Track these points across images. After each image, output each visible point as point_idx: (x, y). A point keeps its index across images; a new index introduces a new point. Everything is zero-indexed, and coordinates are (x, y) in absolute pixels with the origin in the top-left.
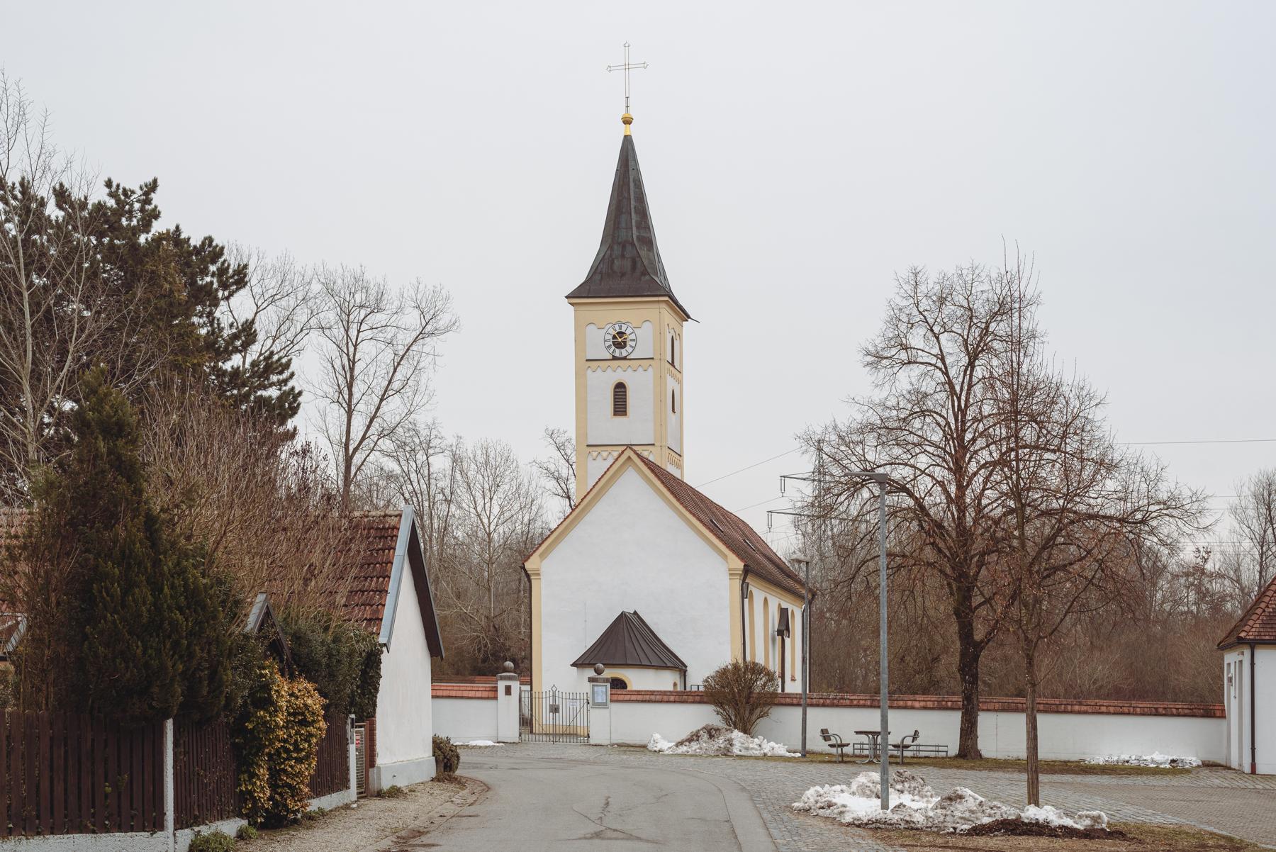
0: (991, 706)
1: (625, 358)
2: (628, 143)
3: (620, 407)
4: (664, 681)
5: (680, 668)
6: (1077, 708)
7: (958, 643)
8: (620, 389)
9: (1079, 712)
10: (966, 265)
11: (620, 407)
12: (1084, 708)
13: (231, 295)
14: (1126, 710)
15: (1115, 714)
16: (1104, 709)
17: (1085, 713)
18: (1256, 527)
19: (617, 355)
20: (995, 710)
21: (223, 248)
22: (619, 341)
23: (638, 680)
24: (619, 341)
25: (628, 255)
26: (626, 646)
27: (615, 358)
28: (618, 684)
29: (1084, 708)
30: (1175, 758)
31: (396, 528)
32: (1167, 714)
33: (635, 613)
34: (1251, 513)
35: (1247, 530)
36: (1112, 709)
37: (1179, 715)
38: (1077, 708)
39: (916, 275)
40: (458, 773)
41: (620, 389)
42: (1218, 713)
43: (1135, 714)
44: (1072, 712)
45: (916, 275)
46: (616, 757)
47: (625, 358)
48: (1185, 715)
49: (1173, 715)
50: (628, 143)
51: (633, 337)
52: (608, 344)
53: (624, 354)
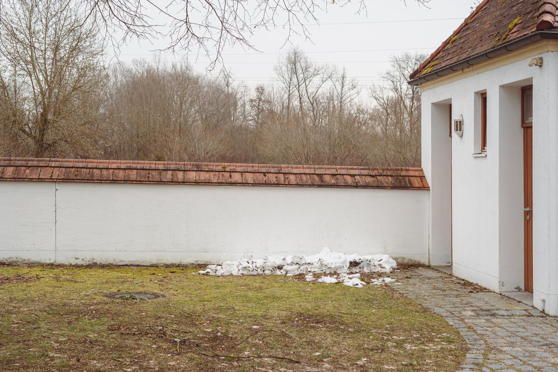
0: (45, 174)
6: (192, 176)
9: (197, 183)
10: (389, 67)
12: (204, 176)
14: (272, 178)
15: (255, 184)
16: (237, 177)
17: (208, 183)
18: (286, 76)
20: (52, 180)
21: (502, 87)
29: (204, 176)
30: (355, 257)
32: (338, 184)
34: (284, 68)
35: (282, 79)
36: (250, 178)
37: (356, 186)
38: (192, 176)
39: (295, 53)
40: (392, 94)
42: (416, 182)
43: (289, 185)
44: (184, 183)
45: (295, 53)
48: (366, 186)
49: (347, 186)
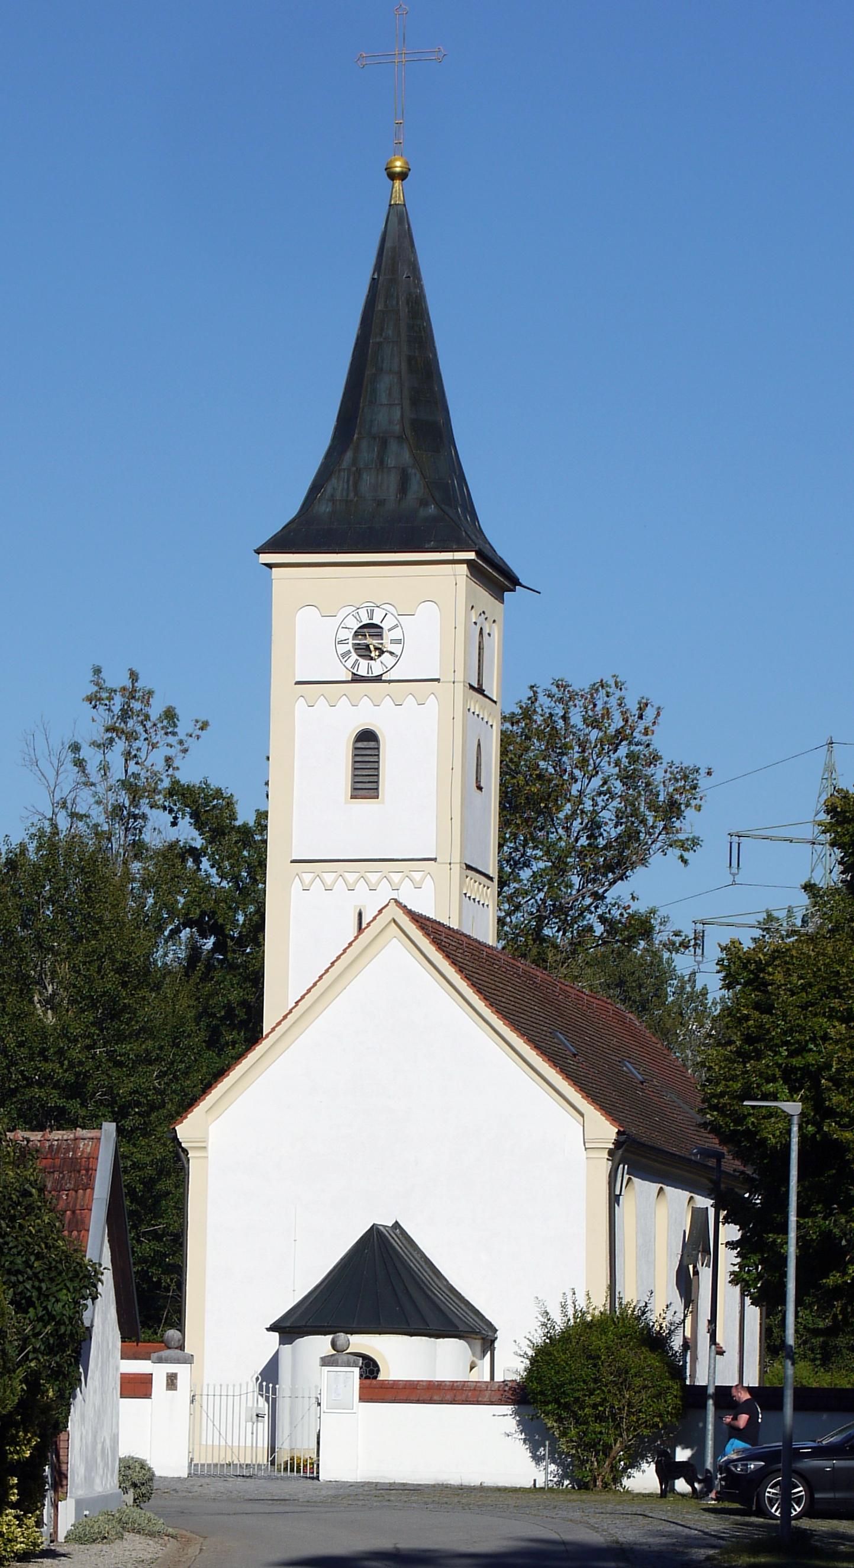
1: (378, 679)
2: (398, 222)
3: (366, 780)
4: (443, 1358)
5: (480, 1334)
7: (815, 1385)
8: (367, 740)
11: (366, 780)
13: (547, 1474)
19: (362, 672)
22: (368, 639)
23: (401, 1355)
24: (368, 639)
25: (391, 462)
26: (380, 1288)
27: (357, 679)
28: (369, 1367)
31: (93, 1157)
33: (397, 1225)
41: (367, 740)
46: (497, 1494)
47: (378, 679)
50: (398, 222)
51: (396, 634)
52: (342, 649)
53: (377, 669)
